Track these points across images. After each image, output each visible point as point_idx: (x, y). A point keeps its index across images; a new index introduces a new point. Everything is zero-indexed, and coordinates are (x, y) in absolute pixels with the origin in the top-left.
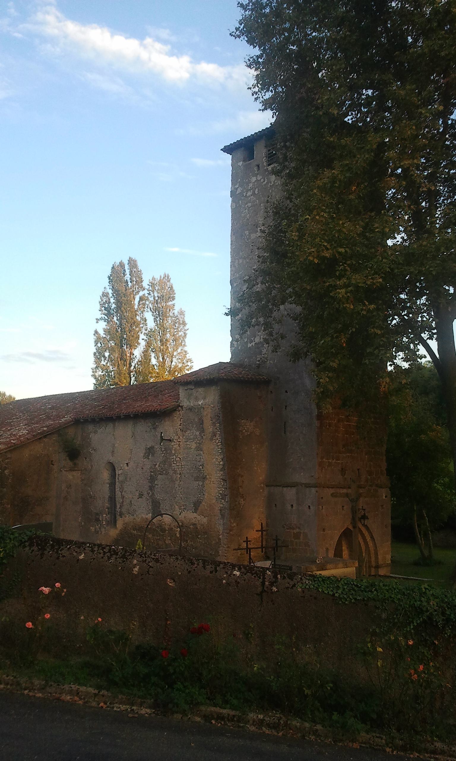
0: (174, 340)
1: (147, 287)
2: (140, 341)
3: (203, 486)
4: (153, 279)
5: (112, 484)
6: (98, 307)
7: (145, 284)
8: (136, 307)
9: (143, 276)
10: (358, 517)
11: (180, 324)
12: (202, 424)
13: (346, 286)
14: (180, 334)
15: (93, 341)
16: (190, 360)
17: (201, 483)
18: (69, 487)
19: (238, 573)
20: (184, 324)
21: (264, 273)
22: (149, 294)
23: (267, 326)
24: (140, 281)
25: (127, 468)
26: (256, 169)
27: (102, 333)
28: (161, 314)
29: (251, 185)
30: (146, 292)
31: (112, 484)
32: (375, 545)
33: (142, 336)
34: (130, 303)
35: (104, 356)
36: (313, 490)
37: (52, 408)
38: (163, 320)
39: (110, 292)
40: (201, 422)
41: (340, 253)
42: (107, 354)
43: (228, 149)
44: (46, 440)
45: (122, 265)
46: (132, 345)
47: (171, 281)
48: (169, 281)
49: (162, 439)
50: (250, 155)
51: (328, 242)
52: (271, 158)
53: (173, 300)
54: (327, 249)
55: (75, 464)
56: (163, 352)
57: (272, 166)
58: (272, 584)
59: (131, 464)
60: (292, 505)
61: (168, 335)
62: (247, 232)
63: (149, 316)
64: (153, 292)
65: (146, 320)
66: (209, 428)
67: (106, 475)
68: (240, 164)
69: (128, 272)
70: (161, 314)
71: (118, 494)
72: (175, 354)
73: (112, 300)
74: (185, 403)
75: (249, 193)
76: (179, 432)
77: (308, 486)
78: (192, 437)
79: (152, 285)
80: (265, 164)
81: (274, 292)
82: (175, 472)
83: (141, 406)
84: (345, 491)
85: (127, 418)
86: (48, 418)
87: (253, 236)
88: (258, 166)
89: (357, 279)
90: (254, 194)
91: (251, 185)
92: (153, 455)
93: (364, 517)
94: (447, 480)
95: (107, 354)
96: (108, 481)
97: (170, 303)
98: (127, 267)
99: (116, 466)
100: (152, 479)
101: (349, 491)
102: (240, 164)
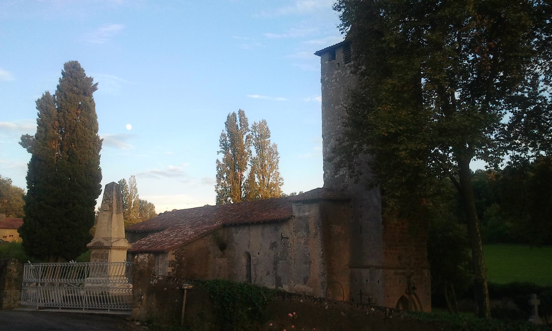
0: (271, 165)
1: (251, 129)
2: (247, 166)
3: (309, 268)
4: (255, 123)
5: (249, 266)
6: (219, 143)
7: (250, 127)
8: (244, 143)
9: (248, 122)
10: (411, 289)
11: (274, 154)
12: (308, 228)
13: (406, 150)
14: (274, 160)
15: (216, 166)
16: (282, 179)
17: (308, 266)
18: (220, 268)
19: (374, 310)
20: (277, 153)
21: (347, 134)
22: (252, 134)
23: (350, 167)
24: (246, 125)
25: (258, 256)
26: (337, 66)
27: (221, 162)
28: (261, 147)
29: (334, 76)
30: (250, 132)
31: (249, 266)
32: (421, 306)
33: (249, 163)
34: (240, 140)
35: (223, 177)
36: (381, 270)
37: (204, 216)
38: (263, 151)
39: (226, 133)
40: (307, 227)
41: (400, 130)
42: (225, 176)
43: (318, 53)
44: (206, 238)
45: (234, 114)
46: (242, 170)
47: (267, 125)
48: (266, 124)
49: (282, 238)
50: (333, 57)
51: (393, 122)
52: (347, 60)
53: (269, 137)
54: (392, 127)
55: (224, 253)
56: (263, 173)
57: (348, 64)
58: (390, 315)
59: (261, 254)
60: (367, 281)
61: (266, 162)
62: (332, 105)
63: (253, 149)
64: (255, 132)
65: (251, 152)
66: (313, 231)
67: (244, 260)
68: (327, 62)
69: (238, 119)
70: (261, 147)
71: (253, 273)
72: (271, 174)
73: (228, 139)
74: (296, 214)
75: (333, 81)
76: (293, 233)
77: (377, 268)
78: (302, 236)
79: (254, 127)
80: (343, 63)
81: (355, 146)
82: (291, 258)
83: (266, 216)
84: (401, 271)
85: (258, 223)
86: (204, 223)
87: (336, 107)
88: (339, 64)
89: (412, 146)
90: (336, 81)
91: (334, 76)
92: (276, 247)
93: (414, 288)
94: (467, 263)
95: (225, 176)
96: (245, 264)
97: (267, 139)
98: (238, 116)
99: (251, 254)
100: (275, 263)
101: (404, 271)
102: (327, 62)
